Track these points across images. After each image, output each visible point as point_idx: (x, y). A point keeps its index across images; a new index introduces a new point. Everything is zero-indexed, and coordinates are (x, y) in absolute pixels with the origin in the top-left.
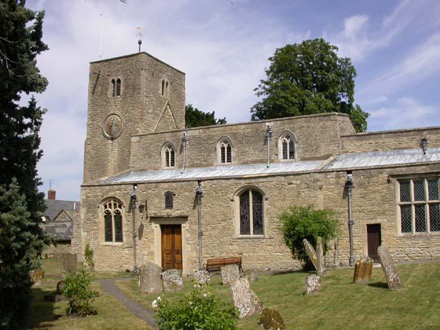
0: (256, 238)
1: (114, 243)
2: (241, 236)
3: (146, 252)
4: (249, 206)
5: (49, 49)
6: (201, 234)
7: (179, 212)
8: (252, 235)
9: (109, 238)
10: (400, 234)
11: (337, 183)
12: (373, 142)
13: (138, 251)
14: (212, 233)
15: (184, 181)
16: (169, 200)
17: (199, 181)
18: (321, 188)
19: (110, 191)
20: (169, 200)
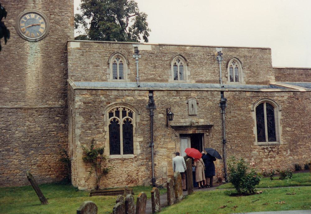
1: (122, 156)
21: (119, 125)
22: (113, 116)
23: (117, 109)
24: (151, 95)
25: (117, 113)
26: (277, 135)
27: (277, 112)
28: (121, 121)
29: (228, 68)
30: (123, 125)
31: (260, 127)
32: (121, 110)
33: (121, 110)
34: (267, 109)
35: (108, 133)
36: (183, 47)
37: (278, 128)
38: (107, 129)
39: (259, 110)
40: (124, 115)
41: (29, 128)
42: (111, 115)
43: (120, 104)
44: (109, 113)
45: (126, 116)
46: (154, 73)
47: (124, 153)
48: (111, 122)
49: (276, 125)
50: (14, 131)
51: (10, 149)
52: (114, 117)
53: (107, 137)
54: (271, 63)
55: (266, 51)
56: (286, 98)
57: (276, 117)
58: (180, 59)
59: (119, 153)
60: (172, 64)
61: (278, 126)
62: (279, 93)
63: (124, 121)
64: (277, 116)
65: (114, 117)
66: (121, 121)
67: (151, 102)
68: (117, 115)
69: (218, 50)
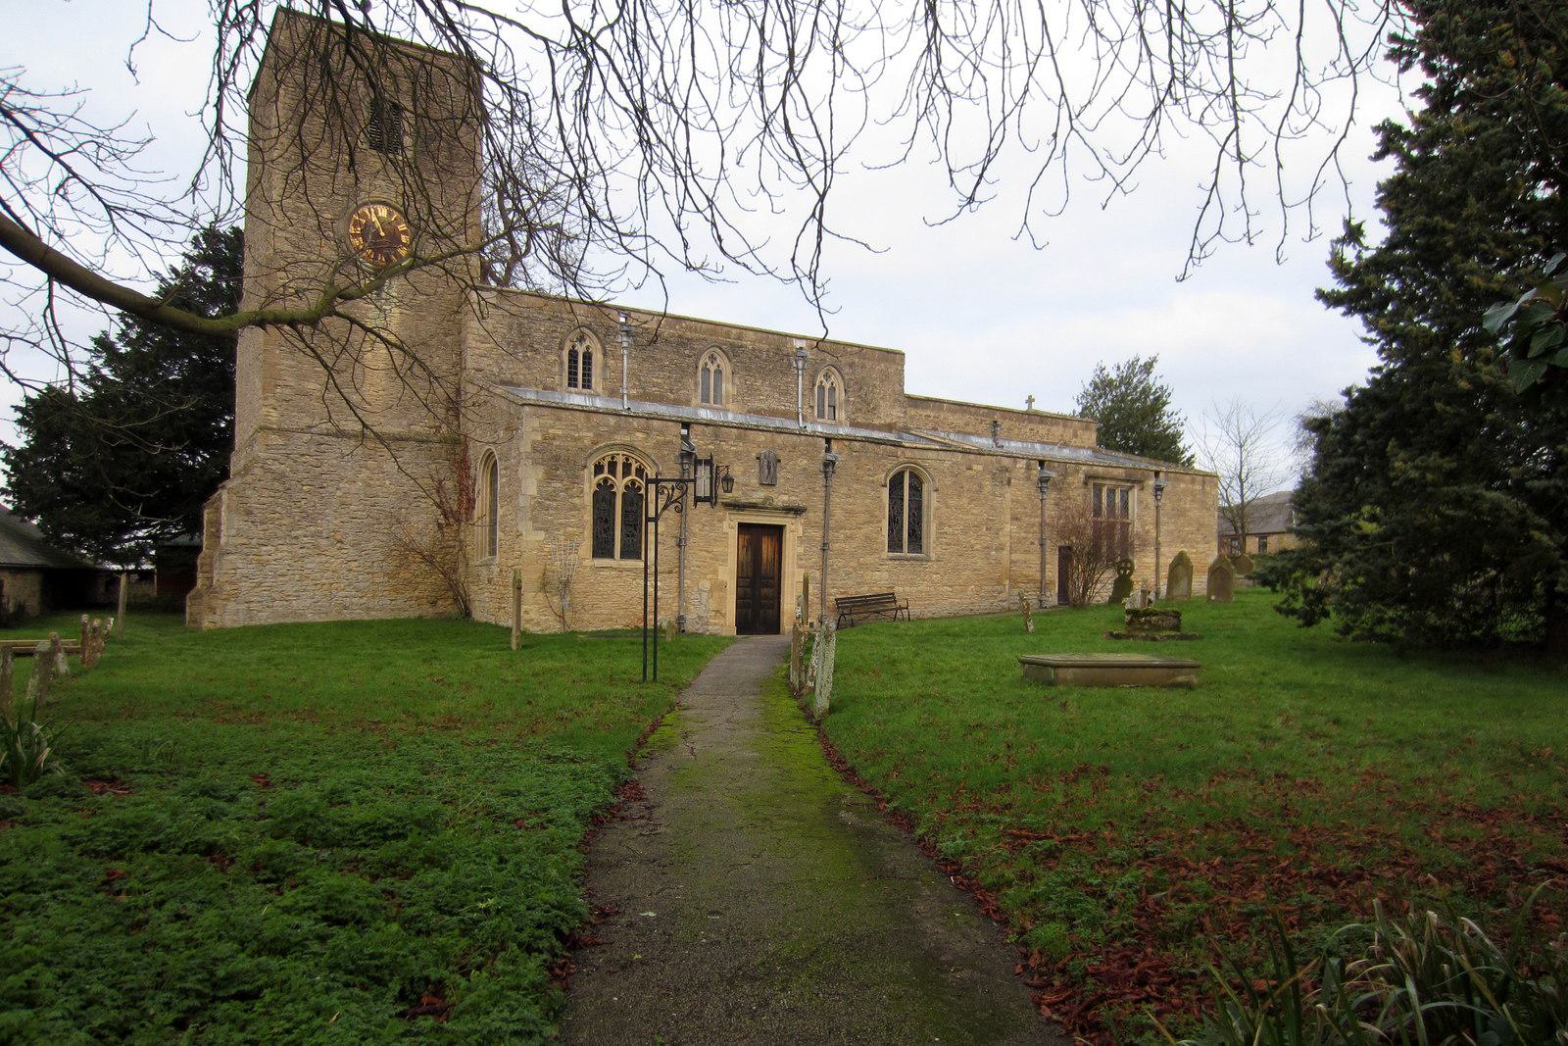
0: (914, 559)
1: (617, 561)
2: (891, 554)
3: (706, 584)
4: (902, 500)
5: (1377, 207)
6: (825, 548)
7: (785, 498)
8: (905, 553)
9: (602, 548)
10: (886, 554)
11: (1028, 478)
12: (932, 414)
13: (687, 582)
14: (847, 547)
15: (707, 425)
16: (769, 468)
17: (828, 440)
18: (1009, 483)
19: (617, 429)
20: (769, 468)
21: (614, 493)
22: (602, 472)
23: (613, 458)
24: (684, 432)
25: (613, 465)
26: (924, 540)
27: (929, 494)
28: (620, 484)
29: (816, 388)
30: (624, 494)
31: (894, 521)
32: (620, 460)
33: (620, 460)
34: (911, 486)
35: (590, 509)
36: (725, 329)
37: (928, 526)
38: (588, 500)
39: (896, 484)
40: (626, 473)
41: (370, 486)
42: (599, 469)
43: (624, 446)
44: (596, 466)
45: (629, 474)
46: (659, 381)
47: (623, 556)
48: (599, 485)
49: (924, 519)
50: (330, 489)
51: (322, 532)
52: (606, 475)
53: (588, 517)
54: (901, 383)
55: (894, 358)
56: (947, 464)
57: (925, 503)
58: (716, 355)
59: (612, 556)
60: (701, 365)
61: (928, 522)
62: (1110, 475)
63: (626, 487)
64: (929, 501)
65: (606, 475)
66: (620, 484)
67: (685, 448)
68: (613, 471)
69: (798, 344)
